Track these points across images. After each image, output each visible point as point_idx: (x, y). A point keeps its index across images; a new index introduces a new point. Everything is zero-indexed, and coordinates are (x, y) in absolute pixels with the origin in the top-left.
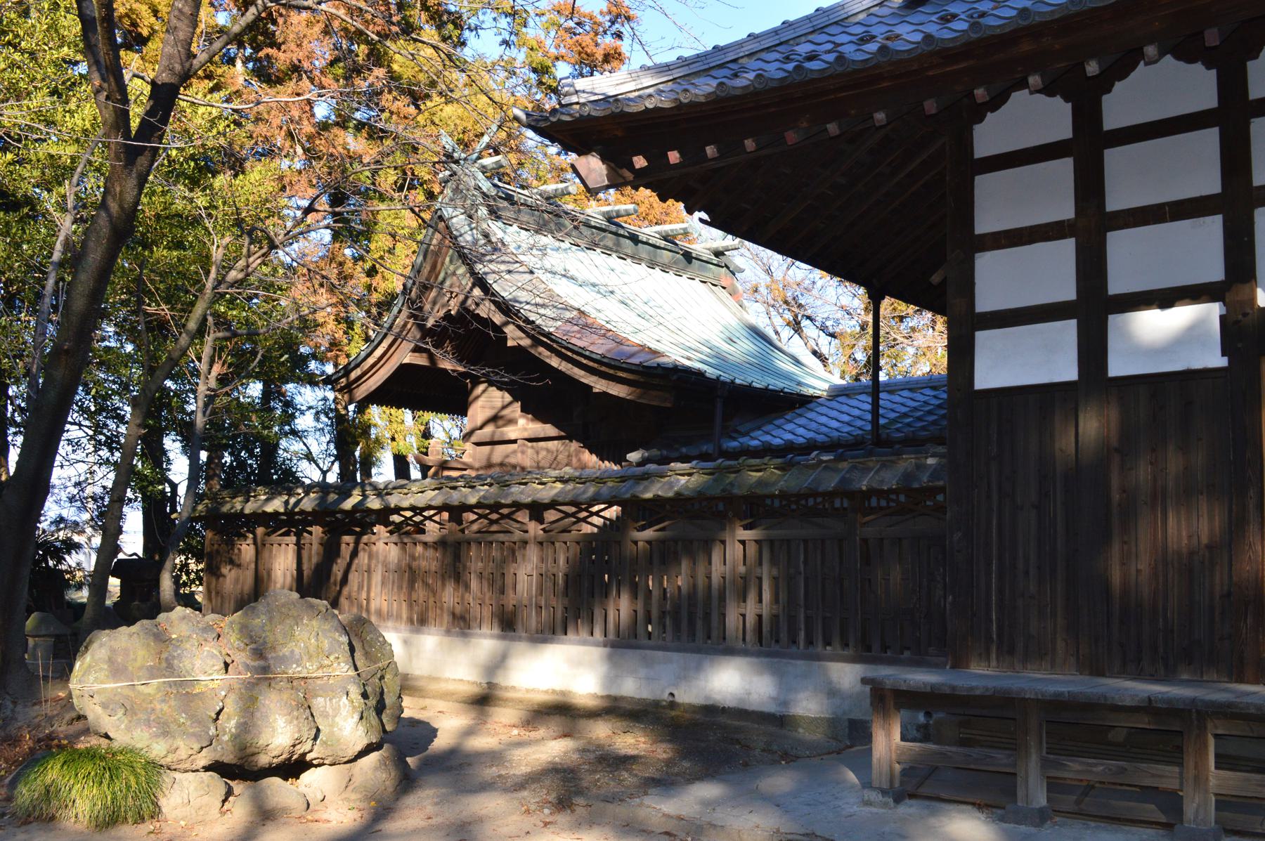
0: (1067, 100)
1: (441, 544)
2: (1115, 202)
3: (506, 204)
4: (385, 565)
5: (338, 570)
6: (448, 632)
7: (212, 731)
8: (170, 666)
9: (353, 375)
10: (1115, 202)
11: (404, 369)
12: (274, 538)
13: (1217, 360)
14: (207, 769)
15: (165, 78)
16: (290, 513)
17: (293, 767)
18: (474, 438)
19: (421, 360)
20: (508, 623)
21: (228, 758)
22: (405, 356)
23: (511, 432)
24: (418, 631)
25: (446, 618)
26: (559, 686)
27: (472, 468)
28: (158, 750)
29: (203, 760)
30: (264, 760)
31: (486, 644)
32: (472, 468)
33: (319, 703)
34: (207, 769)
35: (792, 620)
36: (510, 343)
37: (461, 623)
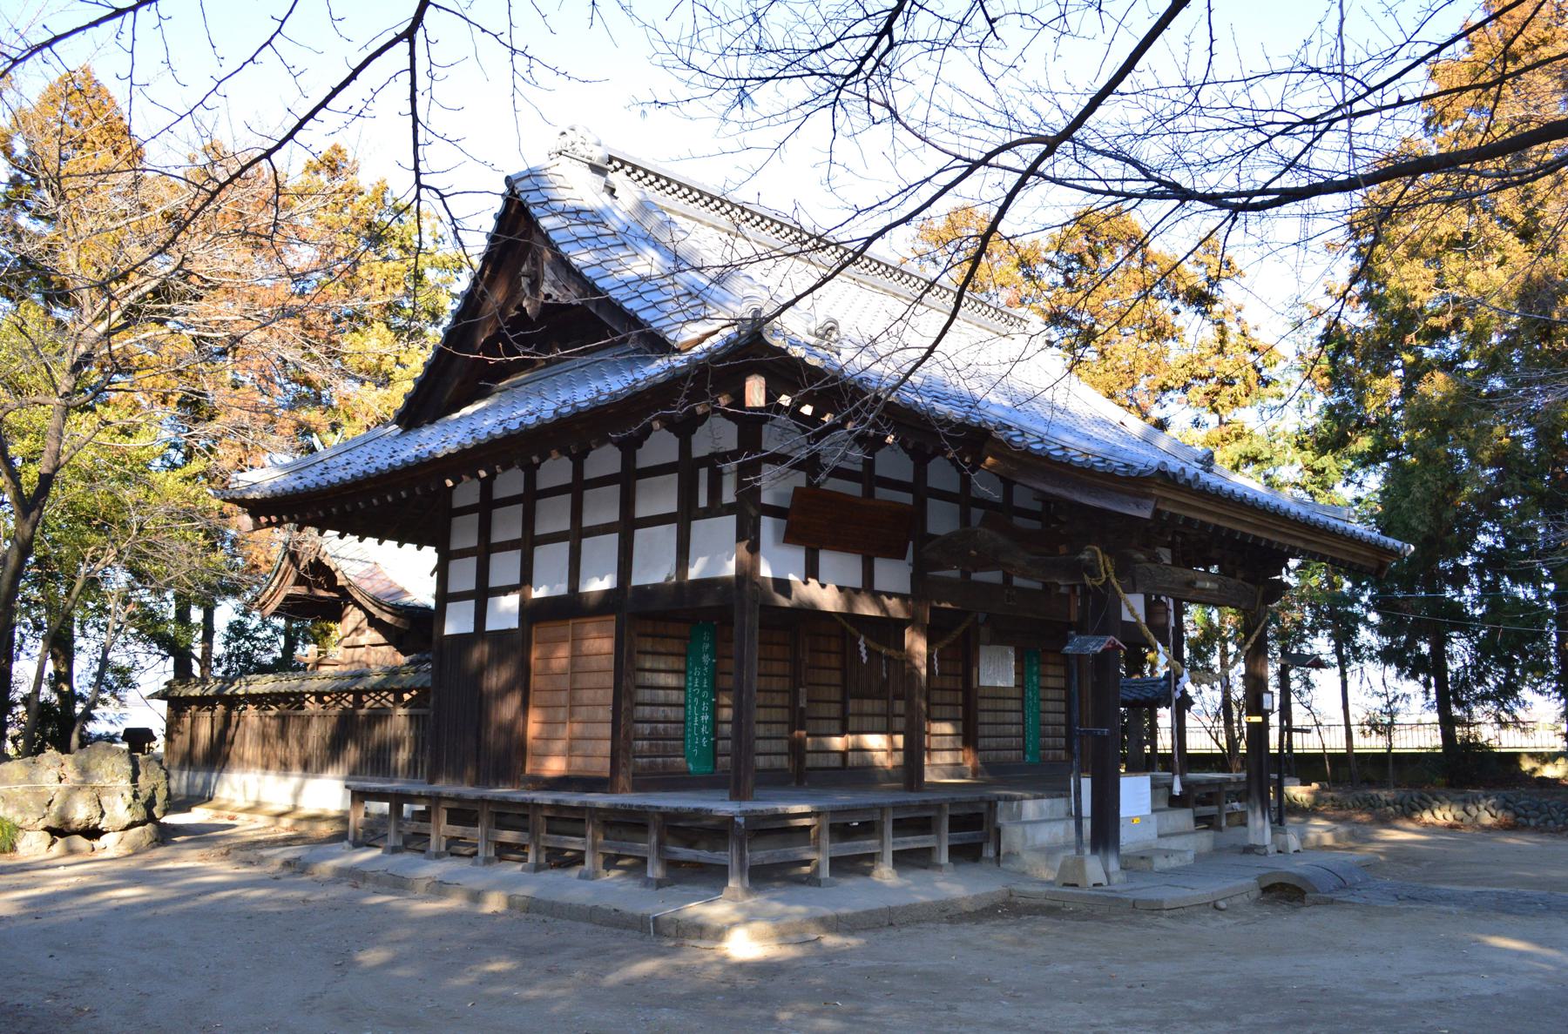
0: (677, 435)
1: (277, 716)
2: (539, 531)
3: (1155, 210)
4: (252, 729)
5: (230, 733)
6: (278, 774)
7: (45, 811)
8: (30, 779)
9: (261, 601)
10: (539, 531)
11: (288, 598)
12: (201, 713)
13: (515, 625)
14: (45, 829)
15: (45, 470)
16: (202, 697)
17: (93, 833)
18: (343, 644)
19: (302, 590)
20: (305, 766)
21: (54, 825)
22: (290, 589)
23: (363, 640)
24: (265, 774)
25: (278, 764)
26: (323, 807)
27: (342, 664)
28: (18, 819)
29: (42, 824)
30: (73, 826)
31: (294, 779)
32: (342, 664)
33: (104, 800)
34: (45, 829)
35: (416, 762)
36: (339, 584)
37: (285, 766)
